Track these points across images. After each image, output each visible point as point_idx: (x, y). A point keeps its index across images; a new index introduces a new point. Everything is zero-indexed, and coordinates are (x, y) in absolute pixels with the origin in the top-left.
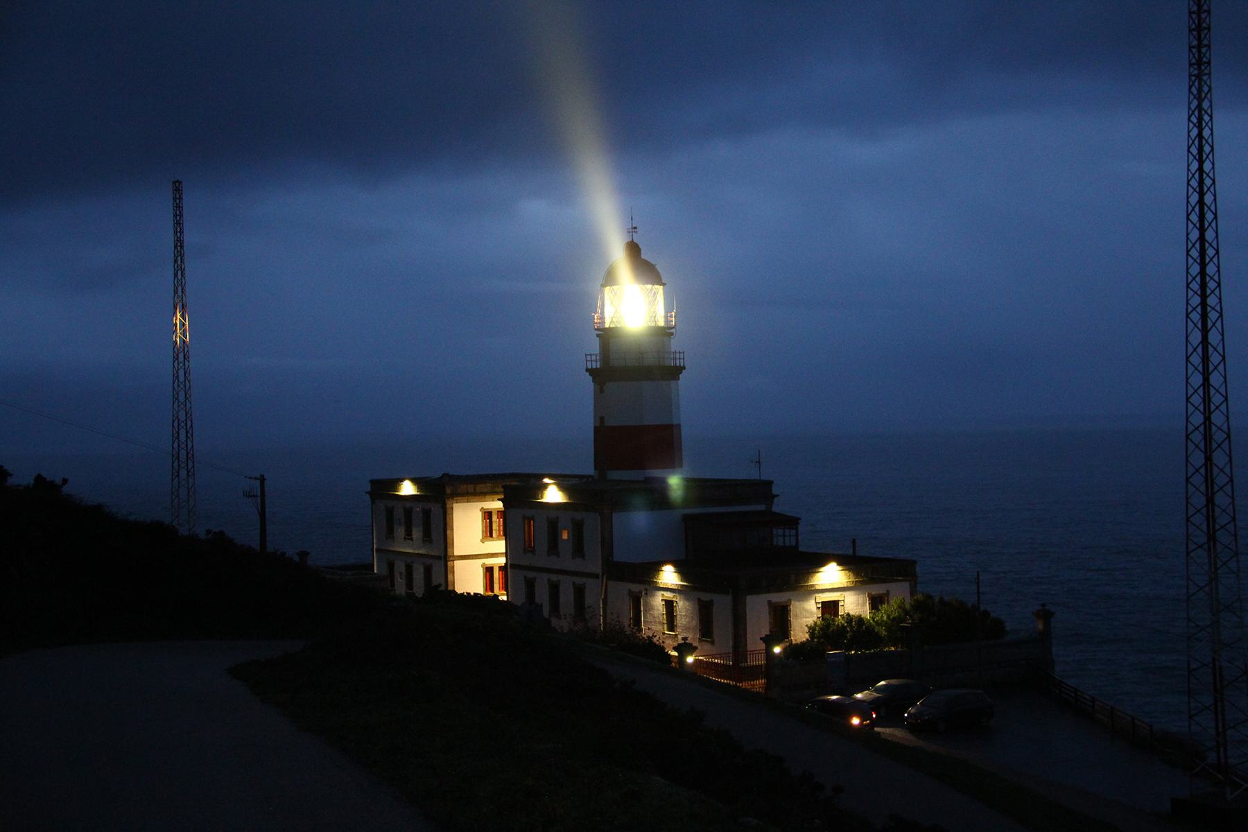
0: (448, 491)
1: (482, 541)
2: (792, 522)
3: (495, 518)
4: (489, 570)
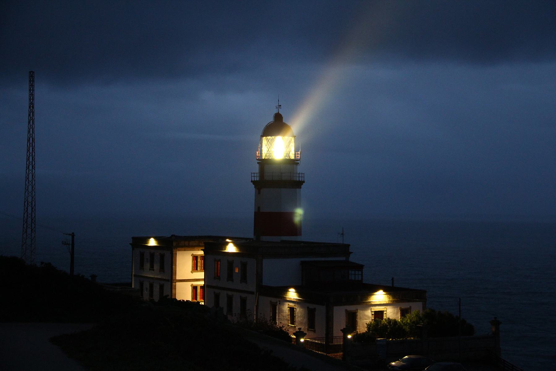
0: (174, 244)
1: (192, 272)
2: (360, 267)
3: (199, 260)
4: (195, 288)
